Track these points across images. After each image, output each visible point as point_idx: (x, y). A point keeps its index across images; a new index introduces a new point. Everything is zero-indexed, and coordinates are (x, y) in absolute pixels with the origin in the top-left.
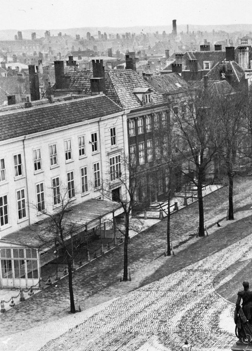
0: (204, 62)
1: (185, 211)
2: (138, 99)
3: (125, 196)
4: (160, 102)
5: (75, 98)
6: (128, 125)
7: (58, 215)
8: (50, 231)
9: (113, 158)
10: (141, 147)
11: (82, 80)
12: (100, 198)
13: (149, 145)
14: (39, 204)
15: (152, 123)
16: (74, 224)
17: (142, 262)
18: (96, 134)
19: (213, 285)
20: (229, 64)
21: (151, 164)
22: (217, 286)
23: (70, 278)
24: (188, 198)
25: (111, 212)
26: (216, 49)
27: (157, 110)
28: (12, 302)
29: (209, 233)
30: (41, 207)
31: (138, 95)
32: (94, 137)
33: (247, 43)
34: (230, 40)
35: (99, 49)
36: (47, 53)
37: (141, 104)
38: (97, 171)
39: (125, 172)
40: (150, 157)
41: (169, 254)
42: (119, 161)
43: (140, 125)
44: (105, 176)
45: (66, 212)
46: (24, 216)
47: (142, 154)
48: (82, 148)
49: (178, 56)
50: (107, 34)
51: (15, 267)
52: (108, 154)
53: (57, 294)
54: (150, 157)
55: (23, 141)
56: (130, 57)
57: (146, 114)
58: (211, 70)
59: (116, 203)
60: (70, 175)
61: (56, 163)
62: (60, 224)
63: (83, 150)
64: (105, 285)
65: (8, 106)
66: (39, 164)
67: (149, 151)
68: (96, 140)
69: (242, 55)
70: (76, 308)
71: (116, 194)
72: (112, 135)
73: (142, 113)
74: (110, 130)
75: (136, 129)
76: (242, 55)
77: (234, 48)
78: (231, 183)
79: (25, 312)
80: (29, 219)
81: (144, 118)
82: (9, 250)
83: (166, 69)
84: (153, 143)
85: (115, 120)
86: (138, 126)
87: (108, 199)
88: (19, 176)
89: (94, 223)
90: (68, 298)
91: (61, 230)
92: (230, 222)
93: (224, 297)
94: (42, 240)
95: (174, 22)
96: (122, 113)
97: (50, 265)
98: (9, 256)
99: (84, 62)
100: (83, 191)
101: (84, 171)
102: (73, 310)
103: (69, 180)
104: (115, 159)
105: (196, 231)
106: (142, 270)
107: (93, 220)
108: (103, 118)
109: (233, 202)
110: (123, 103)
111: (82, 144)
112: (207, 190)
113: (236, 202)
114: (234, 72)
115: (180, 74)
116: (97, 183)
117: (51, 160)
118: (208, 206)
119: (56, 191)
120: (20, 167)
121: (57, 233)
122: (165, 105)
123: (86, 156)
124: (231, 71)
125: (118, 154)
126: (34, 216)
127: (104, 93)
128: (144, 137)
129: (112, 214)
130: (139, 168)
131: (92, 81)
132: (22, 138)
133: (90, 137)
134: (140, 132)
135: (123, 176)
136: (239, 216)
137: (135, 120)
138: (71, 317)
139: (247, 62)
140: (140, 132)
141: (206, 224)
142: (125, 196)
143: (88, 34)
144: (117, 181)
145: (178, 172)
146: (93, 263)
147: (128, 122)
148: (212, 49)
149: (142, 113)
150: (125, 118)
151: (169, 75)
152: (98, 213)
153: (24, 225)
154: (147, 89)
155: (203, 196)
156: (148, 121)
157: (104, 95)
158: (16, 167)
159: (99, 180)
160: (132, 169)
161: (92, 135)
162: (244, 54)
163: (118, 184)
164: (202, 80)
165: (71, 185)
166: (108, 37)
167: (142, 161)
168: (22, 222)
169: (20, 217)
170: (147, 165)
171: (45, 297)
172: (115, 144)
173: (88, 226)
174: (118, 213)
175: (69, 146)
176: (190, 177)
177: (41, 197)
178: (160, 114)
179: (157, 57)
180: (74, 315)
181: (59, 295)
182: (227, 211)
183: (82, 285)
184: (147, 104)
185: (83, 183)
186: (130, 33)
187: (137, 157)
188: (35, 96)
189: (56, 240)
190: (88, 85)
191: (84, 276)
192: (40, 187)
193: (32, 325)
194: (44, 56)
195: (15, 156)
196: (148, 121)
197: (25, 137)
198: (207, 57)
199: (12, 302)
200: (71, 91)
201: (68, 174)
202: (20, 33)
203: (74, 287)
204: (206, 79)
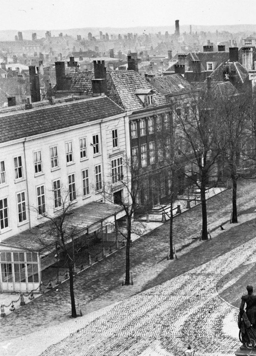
0: (208, 63)
1: (188, 214)
2: (140, 100)
3: (127, 199)
4: (163, 103)
5: (77, 99)
6: (130, 127)
7: (59, 218)
8: (50, 234)
9: (115, 160)
10: (143, 149)
11: (83, 81)
12: (102, 201)
13: (151, 147)
14: (39, 207)
15: (155, 125)
16: (75, 227)
17: (144, 265)
18: (97, 136)
19: (217, 289)
20: (233, 65)
21: (154, 166)
22: (221, 291)
23: (71, 282)
24: (191, 200)
25: (113, 215)
26: (219, 50)
27: (159, 112)
28: (13, 306)
29: (212, 237)
30: (41, 210)
31: (140, 97)
32: (96, 139)
33: (251, 44)
34: (233, 41)
35: (101, 50)
36: (47, 53)
37: (144, 106)
38: (98, 174)
39: (127, 175)
40: (152, 159)
41: (172, 258)
42: (121, 164)
43: (143, 127)
44: (107, 179)
45: (67, 215)
46: (25, 219)
47: (144, 156)
48: (83, 150)
49: (181, 57)
50: (109, 34)
51: (15, 271)
52: (110, 156)
53: (58, 298)
54: (152, 159)
55: (24, 143)
56: (132, 58)
57: (148, 115)
58: (214, 71)
59: (117, 205)
60: (71, 178)
61: (56, 165)
62: (61, 227)
63: (84, 152)
64: (106, 289)
65: (8, 108)
66: (40, 166)
67: (152, 153)
68: (97, 142)
69: (246, 56)
70: (78, 313)
71: (118, 197)
72: (114, 137)
73: (145, 115)
74: (111, 132)
75: (138, 131)
76: (246, 56)
77: (237, 48)
78: (235, 186)
79: (26, 316)
80: (30, 223)
81: (146, 119)
82: (9, 254)
83: (169, 70)
84: (156, 145)
85: (117, 121)
86: (141, 128)
87: (110, 202)
88: (19, 178)
89: (95, 226)
90: (69, 302)
91: (62, 233)
92: (233, 225)
93: (227, 301)
94: (43, 244)
95: (177, 22)
96: (124, 115)
97: (51, 269)
98: (9, 259)
99: (85, 63)
100: (85, 194)
101: (85, 174)
102: (74, 315)
103: (70, 182)
104: (117, 162)
105: (199, 234)
106: (144, 274)
107: (95, 224)
108: (104, 120)
109: (237, 204)
110: (125, 104)
111: (83, 146)
112: (211, 193)
113: (240, 205)
114: (237, 73)
115: (183, 75)
116: (99, 186)
117: (52, 162)
118: (211, 209)
119: (57, 193)
120: (20, 169)
121: (58, 236)
122: (167, 106)
123: (87, 159)
124: (235, 72)
125: (120, 157)
126: (34, 219)
127: (105, 94)
128: (146, 139)
129: (113, 217)
130: (141, 170)
131: (94, 82)
132: (22, 140)
133: (92, 138)
134: (143, 134)
135: (125, 179)
136: (242, 219)
137: (138, 121)
138: (72, 321)
139: (250, 63)
140: (143, 134)
141: (210, 227)
142: (127, 199)
143: (90, 34)
144: (119, 183)
145: (181, 175)
146: (95, 266)
147: (130, 124)
148: (216, 50)
149: (145, 115)
150: (127, 120)
151: (172, 76)
152: (99, 216)
153: (25, 228)
154: (150, 90)
155: (206, 198)
156: (150, 123)
157: (106, 96)
158: (16, 170)
159: (101, 183)
160: (134, 171)
161: (94, 137)
162: (247, 55)
163: (120, 186)
164: (205, 82)
165: (72, 188)
166: (110, 38)
167: (144, 163)
168: (22, 225)
169: (20, 221)
170: (150, 168)
171: (46, 302)
172: (116, 146)
173: (90, 229)
174: (120, 216)
175: (70, 148)
176: (193, 179)
177: (41, 200)
178: (162, 116)
179: (160, 58)
180: (75, 319)
181: (60, 299)
182: (230, 214)
183: (84, 289)
184: (149, 106)
185: (84, 186)
186: (132, 34)
187: (140, 159)
188: (36, 97)
189: (57, 243)
190: (90, 86)
191: (86, 280)
192: (41, 190)
193: (32, 330)
194: (45, 56)
195: (15, 159)
196: (150, 123)
197: (25, 139)
198: (211, 58)
199: (13, 306)
200: (72, 93)
201: (70, 177)
202: (20, 34)
203: (75, 291)
204: (209, 80)
